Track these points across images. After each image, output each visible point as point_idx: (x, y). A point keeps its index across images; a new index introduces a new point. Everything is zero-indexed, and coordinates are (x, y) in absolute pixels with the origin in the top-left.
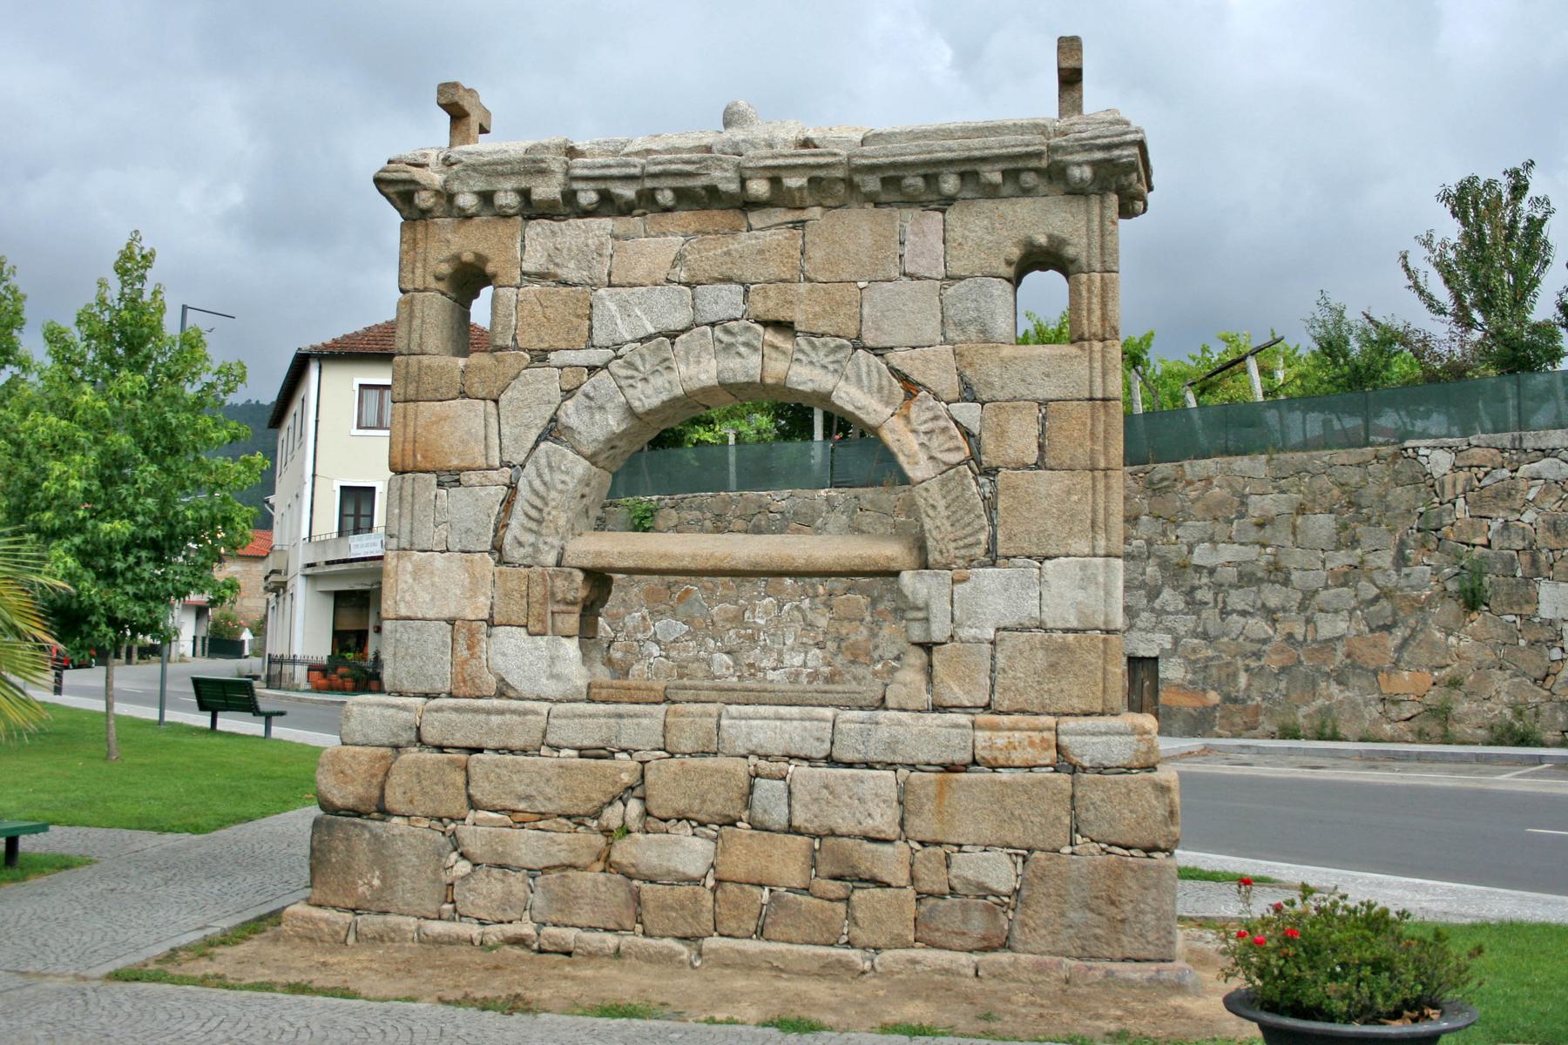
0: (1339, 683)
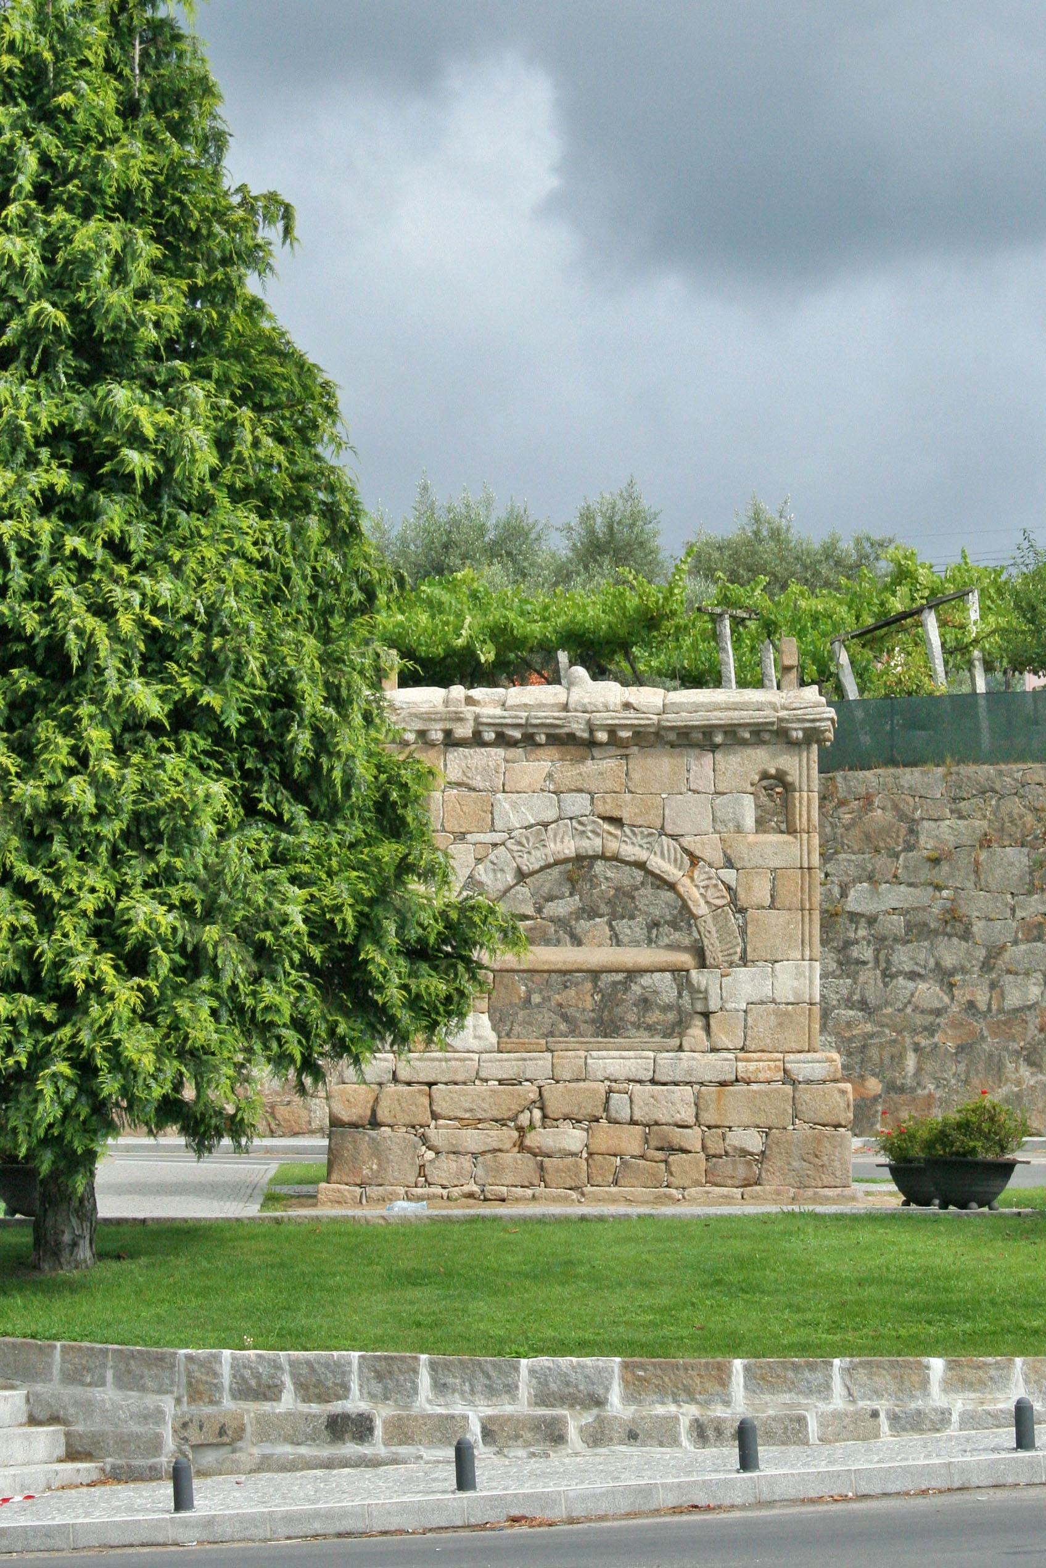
0: (1031, 1063)
